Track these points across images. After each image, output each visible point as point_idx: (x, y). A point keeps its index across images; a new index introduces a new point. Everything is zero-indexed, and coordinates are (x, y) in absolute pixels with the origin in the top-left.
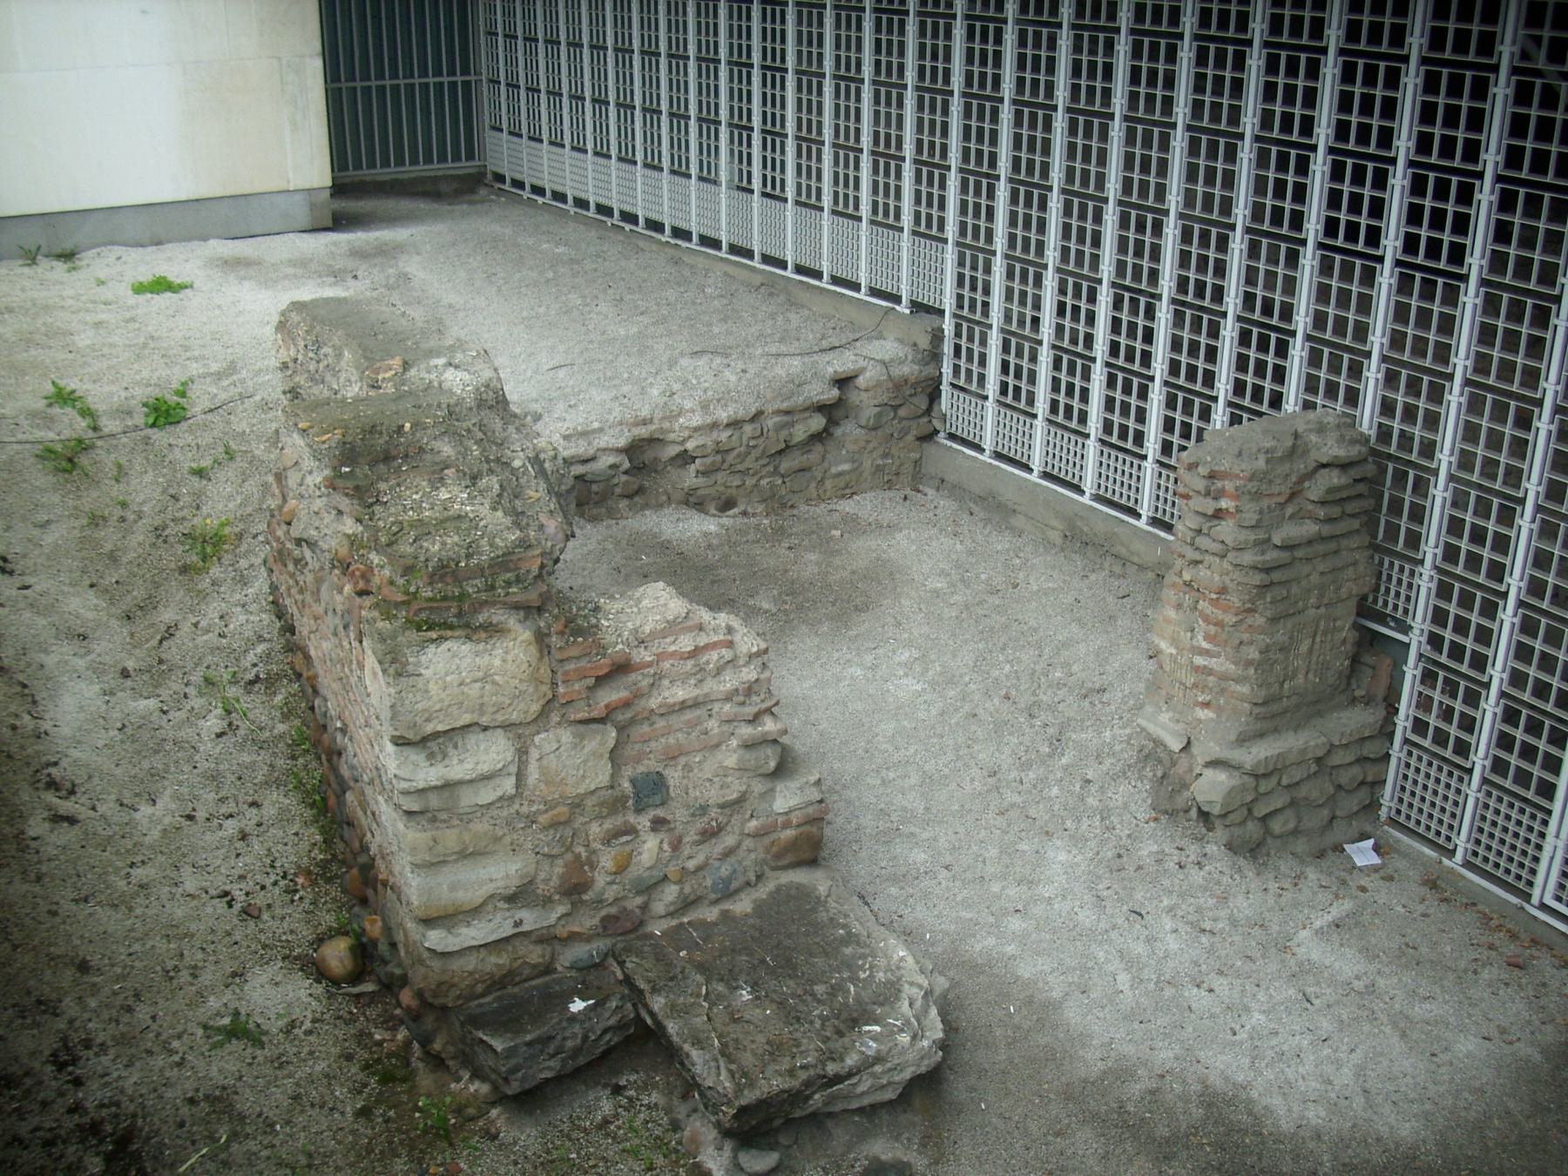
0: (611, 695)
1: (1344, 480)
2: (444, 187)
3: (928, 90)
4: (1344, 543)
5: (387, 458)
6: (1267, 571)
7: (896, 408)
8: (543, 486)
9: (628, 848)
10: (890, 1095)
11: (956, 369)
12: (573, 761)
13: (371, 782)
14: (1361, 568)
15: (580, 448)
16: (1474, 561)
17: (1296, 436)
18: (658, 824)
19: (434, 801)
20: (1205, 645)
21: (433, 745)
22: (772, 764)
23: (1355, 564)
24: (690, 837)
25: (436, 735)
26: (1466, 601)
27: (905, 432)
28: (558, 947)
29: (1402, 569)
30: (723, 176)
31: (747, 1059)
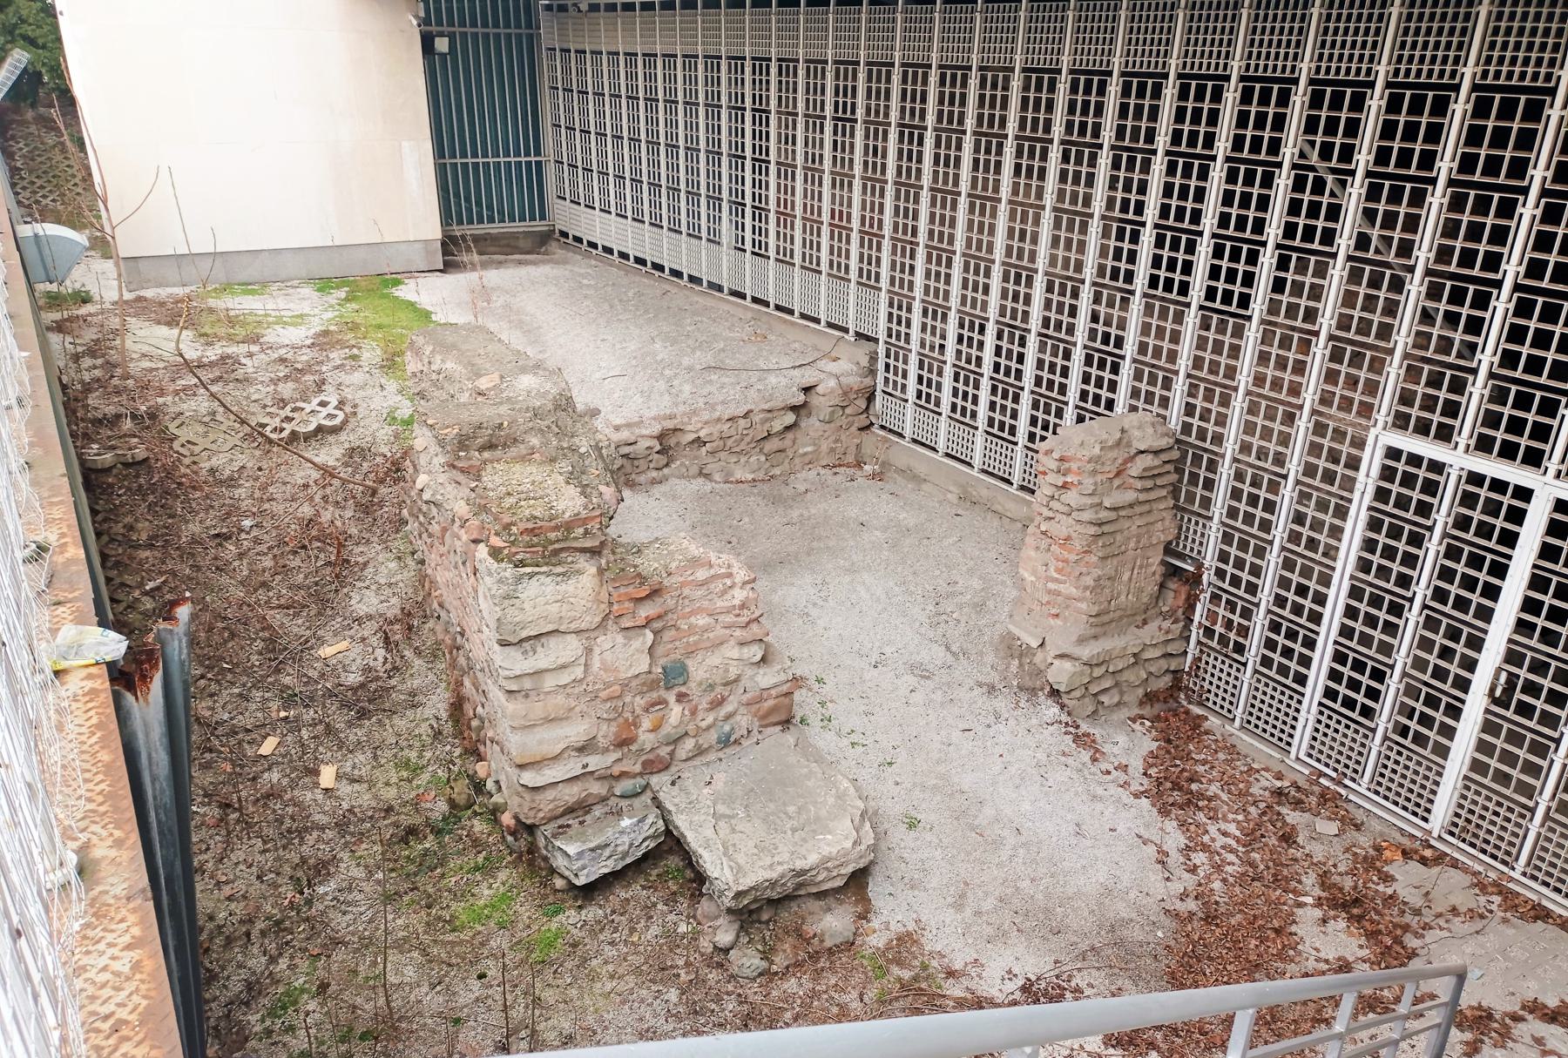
0: (646, 611)
1: (1157, 462)
2: (522, 243)
3: (870, 179)
4: (1155, 506)
5: (491, 446)
6: (1100, 525)
10: (839, 883)
11: (887, 380)
12: (626, 656)
13: (482, 670)
14: (1167, 523)
15: (625, 435)
16: (1249, 519)
17: (1123, 431)
18: (681, 697)
19: (527, 684)
20: (1056, 575)
21: (526, 645)
22: (758, 657)
24: (704, 705)
25: (529, 638)
26: (1243, 546)
27: (851, 424)
29: (1197, 523)
30: (724, 241)
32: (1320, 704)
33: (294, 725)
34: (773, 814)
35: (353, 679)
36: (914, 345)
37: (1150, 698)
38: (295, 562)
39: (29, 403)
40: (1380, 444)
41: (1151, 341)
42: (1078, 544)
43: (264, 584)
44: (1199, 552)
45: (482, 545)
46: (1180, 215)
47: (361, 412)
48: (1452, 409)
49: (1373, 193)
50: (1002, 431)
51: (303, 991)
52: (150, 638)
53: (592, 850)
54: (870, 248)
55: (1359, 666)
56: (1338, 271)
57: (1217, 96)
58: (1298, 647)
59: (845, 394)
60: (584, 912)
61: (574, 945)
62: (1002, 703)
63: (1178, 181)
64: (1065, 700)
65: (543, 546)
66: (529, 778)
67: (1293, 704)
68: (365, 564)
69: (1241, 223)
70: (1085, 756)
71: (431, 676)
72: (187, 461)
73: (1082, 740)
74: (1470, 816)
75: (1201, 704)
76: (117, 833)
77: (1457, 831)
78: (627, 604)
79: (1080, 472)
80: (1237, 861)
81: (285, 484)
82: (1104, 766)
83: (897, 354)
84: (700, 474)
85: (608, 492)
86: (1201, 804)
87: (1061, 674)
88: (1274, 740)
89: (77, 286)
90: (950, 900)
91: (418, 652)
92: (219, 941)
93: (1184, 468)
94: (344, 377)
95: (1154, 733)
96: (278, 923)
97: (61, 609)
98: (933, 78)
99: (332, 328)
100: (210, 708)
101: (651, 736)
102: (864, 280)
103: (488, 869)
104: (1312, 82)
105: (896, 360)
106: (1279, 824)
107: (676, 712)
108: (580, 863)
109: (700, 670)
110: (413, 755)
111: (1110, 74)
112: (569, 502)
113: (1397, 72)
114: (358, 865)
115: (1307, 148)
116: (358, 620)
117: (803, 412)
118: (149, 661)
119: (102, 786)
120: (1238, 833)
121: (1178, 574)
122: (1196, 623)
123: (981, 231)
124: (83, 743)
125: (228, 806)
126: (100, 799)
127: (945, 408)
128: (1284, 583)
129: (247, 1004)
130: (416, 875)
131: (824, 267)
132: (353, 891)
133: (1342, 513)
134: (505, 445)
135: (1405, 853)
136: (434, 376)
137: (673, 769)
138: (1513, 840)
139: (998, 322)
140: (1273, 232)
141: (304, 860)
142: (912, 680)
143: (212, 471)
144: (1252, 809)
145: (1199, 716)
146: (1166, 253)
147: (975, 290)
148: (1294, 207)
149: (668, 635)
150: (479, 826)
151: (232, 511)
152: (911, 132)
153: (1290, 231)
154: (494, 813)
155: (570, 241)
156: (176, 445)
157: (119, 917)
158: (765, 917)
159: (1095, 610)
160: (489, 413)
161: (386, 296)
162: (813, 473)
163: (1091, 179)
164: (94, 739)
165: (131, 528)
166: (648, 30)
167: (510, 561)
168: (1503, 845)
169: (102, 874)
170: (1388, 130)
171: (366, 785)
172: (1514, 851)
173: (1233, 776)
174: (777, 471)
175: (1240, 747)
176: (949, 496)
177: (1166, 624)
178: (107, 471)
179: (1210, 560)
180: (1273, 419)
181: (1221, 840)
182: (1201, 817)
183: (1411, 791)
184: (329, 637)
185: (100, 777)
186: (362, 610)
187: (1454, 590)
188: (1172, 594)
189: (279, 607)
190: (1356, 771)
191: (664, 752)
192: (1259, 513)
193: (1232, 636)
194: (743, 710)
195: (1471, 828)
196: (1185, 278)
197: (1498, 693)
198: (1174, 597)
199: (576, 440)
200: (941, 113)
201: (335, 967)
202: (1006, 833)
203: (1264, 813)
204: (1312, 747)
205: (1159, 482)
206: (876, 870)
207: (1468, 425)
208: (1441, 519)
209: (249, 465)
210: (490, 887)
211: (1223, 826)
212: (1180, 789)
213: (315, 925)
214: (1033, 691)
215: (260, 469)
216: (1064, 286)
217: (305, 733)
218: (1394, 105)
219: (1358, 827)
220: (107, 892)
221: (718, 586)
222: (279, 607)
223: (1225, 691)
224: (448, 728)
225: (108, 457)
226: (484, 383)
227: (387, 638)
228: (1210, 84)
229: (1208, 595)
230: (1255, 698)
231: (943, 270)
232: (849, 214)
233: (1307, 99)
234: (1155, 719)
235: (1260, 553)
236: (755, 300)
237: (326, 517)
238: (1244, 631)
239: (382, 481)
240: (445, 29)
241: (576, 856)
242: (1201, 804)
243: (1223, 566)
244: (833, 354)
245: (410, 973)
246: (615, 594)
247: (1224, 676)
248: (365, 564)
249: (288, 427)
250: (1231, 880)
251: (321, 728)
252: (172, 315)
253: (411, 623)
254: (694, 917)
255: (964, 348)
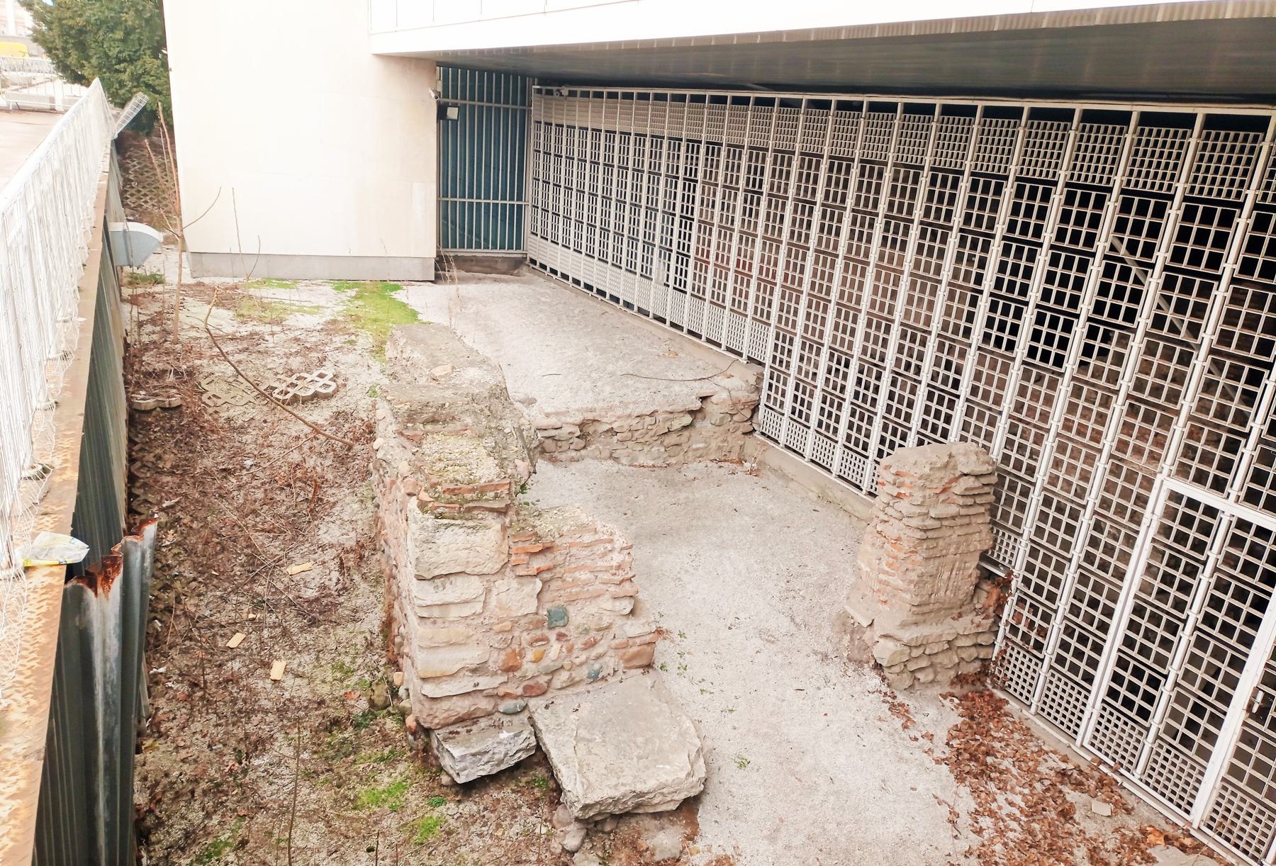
0: (539, 563)
1: (977, 484)
2: (499, 266)
4: (974, 520)
5: (434, 421)
7: (732, 415)
8: (520, 443)
9: (542, 648)
10: (673, 807)
11: (769, 396)
12: (518, 598)
14: (984, 535)
15: (553, 421)
16: (1053, 539)
17: (950, 456)
18: (560, 637)
19: (436, 613)
22: (628, 611)
23: (980, 532)
24: (579, 645)
25: (441, 576)
26: (1047, 560)
27: (736, 429)
28: (499, 701)
29: (1009, 538)
31: (592, 777)
32: (1104, 701)
33: (258, 625)
34: (624, 742)
35: (310, 594)
36: (793, 371)
37: (960, 679)
38: (281, 496)
39: (72, 358)
40: (1164, 488)
41: (982, 386)
42: (906, 545)
43: (254, 511)
44: (1010, 562)
45: (414, 498)
46: (1011, 286)
47: (350, 384)
48: (1226, 465)
49: (1169, 284)
50: (857, 447)
51: (227, 844)
52: (117, 548)
53: (474, 755)
54: (765, 292)
55: (1138, 673)
56: (1137, 344)
57: (1046, 196)
58: (1087, 651)
59: (734, 404)
60: (461, 806)
61: (449, 833)
62: (833, 671)
63: (1011, 260)
64: (886, 673)
65: (459, 504)
66: (430, 690)
67: (1081, 698)
68: (335, 504)
69: (1060, 298)
70: (898, 723)
71: (372, 598)
72: (210, 410)
73: (897, 708)
74: (1226, 814)
75: (1003, 689)
76: (33, 702)
77: (1214, 825)
78: (523, 557)
79: (912, 486)
80: (1019, 829)
81: (282, 434)
82: (913, 733)
83: (779, 377)
84: (611, 457)
85: (523, 466)
86: (993, 775)
87: (884, 651)
88: (1064, 728)
89: (155, 271)
90: (765, 832)
91: (364, 577)
92: (169, 795)
93: (1000, 493)
94: (341, 357)
95: (961, 710)
96: (218, 785)
97: (47, 518)
98: (824, 165)
99: (340, 318)
100: (197, 605)
101: (533, 666)
102: (758, 317)
103: (390, 761)
104: (1123, 191)
105: (778, 381)
106: (1059, 801)
107: (555, 649)
108: (462, 765)
109: (579, 616)
110: (348, 660)
111: (886, 164)
112: (487, 471)
113: (1192, 189)
114: (289, 745)
115: (1117, 243)
116: (322, 547)
117: (699, 415)
118: (112, 566)
119: (34, 663)
120: (1022, 805)
121: (990, 576)
122: (1003, 620)
123: (852, 286)
124: (30, 626)
125: (196, 685)
126: (29, 673)
127: (813, 423)
128: (1079, 596)
129: (183, 849)
130: (333, 759)
131: (728, 304)
132: (280, 769)
133: (1130, 541)
134: (445, 421)
135: (1167, 839)
136: (404, 362)
137: (549, 695)
138: (1263, 839)
139: (860, 359)
140: (1086, 308)
141: (247, 736)
142: (758, 643)
143: (229, 420)
144: (1038, 785)
145: (1001, 700)
146: (998, 316)
147: (844, 332)
148: (1104, 289)
149: (555, 585)
150: (390, 724)
151: (239, 453)
152: (805, 205)
153: (1099, 307)
154: (403, 714)
155: (537, 267)
156: (204, 398)
157: (13, 771)
158: (608, 828)
159: (917, 601)
160: (437, 395)
161: (384, 297)
162: (702, 465)
163: (941, 253)
164: (39, 624)
165: (159, 458)
166: (717, 122)
167: (432, 513)
168: (1254, 843)
169: (11, 734)
170: (1183, 235)
171: (306, 681)
172: (1263, 849)
173: (1024, 755)
174: (673, 461)
175: (1033, 730)
176: (810, 494)
177: (978, 619)
178: (149, 412)
179: (1019, 570)
180: (1077, 458)
181: (1008, 809)
182: (992, 787)
183: (1177, 785)
184: (297, 558)
185: (34, 655)
186: (325, 538)
187: (1221, 616)
188: (985, 594)
189: (263, 530)
190: (1131, 763)
191: (543, 680)
192: (1061, 535)
193: (1033, 635)
194: (611, 653)
195: (1227, 824)
196: (1012, 338)
197: (1255, 709)
198: (987, 597)
199: (503, 422)
200: (858, 198)
201: (254, 828)
202: (821, 781)
203: (1047, 790)
204: (1095, 738)
205: (979, 500)
206: (707, 800)
207: (1239, 480)
208: (1214, 555)
209: (257, 418)
210: (390, 776)
211: (1011, 797)
212: (977, 760)
213: (247, 791)
214: (860, 663)
215: (265, 422)
216: (914, 335)
217: (266, 633)
218: (1189, 215)
219: (1128, 812)
220: (9, 749)
221: (600, 549)
222: (263, 530)
223: (1025, 681)
224: (379, 641)
225: (151, 402)
226: (438, 372)
227: (342, 563)
228: (1041, 187)
229: (1015, 599)
230: (1049, 689)
231: (820, 314)
232: (751, 265)
233: (1118, 205)
234: (964, 698)
235: (1060, 568)
236: (673, 325)
237: (310, 463)
238: (1043, 632)
239: (358, 440)
240: (459, 102)
241: (461, 759)
242: (993, 775)
243: (1029, 576)
244: (729, 373)
245: (314, 840)
246: (514, 547)
247: (1024, 668)
248: (335, 504)
249: (292, 391)
250: (1012, 844)
251: (279, 630)
252: (225, 299)
253: (363, 554)
254: (551, 821)
255: (832, 377)
